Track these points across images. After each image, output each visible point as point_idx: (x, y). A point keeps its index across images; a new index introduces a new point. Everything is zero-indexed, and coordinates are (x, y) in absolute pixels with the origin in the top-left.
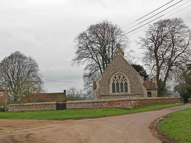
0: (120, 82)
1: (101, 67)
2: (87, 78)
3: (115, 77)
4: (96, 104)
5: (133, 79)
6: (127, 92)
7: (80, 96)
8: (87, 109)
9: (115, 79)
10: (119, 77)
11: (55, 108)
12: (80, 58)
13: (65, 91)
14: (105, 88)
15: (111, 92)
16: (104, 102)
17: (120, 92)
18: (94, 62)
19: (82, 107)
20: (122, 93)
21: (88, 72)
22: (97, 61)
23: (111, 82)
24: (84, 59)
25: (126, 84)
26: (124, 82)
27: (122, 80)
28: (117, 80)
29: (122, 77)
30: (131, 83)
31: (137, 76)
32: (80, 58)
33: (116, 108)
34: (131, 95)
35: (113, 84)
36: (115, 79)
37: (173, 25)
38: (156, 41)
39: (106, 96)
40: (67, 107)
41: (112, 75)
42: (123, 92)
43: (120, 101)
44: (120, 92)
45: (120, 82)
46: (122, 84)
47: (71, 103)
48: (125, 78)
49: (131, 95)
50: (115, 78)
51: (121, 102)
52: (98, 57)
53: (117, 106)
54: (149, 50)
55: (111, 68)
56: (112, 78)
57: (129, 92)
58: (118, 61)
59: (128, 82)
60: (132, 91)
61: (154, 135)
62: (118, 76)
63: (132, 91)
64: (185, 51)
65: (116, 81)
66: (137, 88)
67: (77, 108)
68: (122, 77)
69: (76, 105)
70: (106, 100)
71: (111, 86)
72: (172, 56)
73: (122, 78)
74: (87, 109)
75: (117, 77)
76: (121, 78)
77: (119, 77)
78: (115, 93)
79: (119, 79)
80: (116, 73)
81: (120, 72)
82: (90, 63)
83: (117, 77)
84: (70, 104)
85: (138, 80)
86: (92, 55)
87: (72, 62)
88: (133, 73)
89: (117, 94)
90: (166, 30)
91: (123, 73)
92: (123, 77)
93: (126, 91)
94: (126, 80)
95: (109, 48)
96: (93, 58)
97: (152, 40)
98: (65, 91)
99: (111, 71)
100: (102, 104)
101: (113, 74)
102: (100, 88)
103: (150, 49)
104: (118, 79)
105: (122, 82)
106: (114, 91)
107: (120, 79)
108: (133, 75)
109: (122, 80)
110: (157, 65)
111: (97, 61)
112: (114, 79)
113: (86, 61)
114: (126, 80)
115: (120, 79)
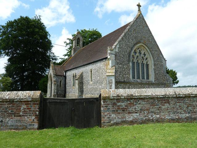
14: (124, 67)
25: (147, 65)
26: (145, 62)
30: (155, 65)
55: (132, 34)
68: (143, 52)
77: (140, 53)
84: (123, 104)
89: (138, 80)
99: (132, 40)
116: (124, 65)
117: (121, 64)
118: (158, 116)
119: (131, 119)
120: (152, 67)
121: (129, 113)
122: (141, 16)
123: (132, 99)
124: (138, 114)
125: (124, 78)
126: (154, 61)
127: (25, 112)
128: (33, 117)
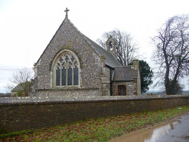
5: (87, 61)
10: (67, 59)
17: (67, 84)
20: (67, 86)
23: (55, 69)
25: (76, 69)
26: (73, 67)
27: (70, 62)
30: (81, 67)
31: (94, 54)
35: (58, 71)
36: (61, 62)
37: (182, 20)
38: (164, 39)
44: (67, 84)
46: (64, 70)
54: (157, 48)
55: (54, 44)
60: (83, 82)
66: (92, 77)
68: (69, 57)
72: (182, 54)
75: (64, 58)
77: (67, 59)
78: (71, 86)
81: (66, 50)
85: (94, 62)
88: (86, 50)
90: (174, 25)
99: (54, 50)
103: (158, 47)
106: (58, 84)
108: (86, 53)
110: (166, 62)
115: (67, 61)
122: (66, 21)
125: (45, 86)
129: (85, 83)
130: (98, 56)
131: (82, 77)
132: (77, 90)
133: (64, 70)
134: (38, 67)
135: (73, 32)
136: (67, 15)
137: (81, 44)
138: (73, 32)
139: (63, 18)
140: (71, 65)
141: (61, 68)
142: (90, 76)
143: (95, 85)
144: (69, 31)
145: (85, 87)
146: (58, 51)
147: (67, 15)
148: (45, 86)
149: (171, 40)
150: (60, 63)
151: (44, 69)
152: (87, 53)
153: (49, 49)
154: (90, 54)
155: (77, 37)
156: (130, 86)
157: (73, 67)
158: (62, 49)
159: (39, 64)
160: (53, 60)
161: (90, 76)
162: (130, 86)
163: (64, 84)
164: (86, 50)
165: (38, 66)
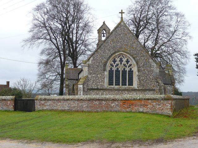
0: (121, 69)
1: (62, 52)
2: (44, 65)
3: (115, 59)
4: (97, 103)
5: (144, 65)
6: (132, 85)
7: (33, 92)
8: (77, 111)
9: (114, 63)
10: (121, 61)
11: (11, 107)
12: (35, 37)
13: (8, 83)
14: (98, 77)
15: (106, 84)
16: (114, 100)
18: (54, 47)
19: (67, 108)
20: (121, 86)
21: (44, 58)
22: (56, 45)
23: (108, 69)
24: (40, 41)
25: (131, 72)
26: (127, 69)
27: (124, 65)
28: (117, 65)
29: (125, 60)
30: (139, 71)
32: (35, 37)
33: (140, 112)
34: (139, 90)
35: (111, 72)
36: (114, 63)
39: (97, 89)
40: (37, 106)
41: (110, 57)
42: (126, 85)
43: (148, 99)
45: (121, 69)
46: (117, 71)
47: (45, 99)
48: (129, 63)
49: (139, 90)
50: (115, 61)
51: (150, 101)
52: (58, 40)
53: (141, 110)
55: (109, 45)
56: (109, 61)
57: (135, 85)
58: (120, 35)
59: (135, 69)
61: (27, 143)
62: (119, 59)
63: (140, 84)
64: (170, 40)
65: (116, 66)
66: (149, 80)
67: (56, 110)
68: (125, 60)
69: (54, 103)
70: (117, 97)
71: (106, 73)
72: (156, 45)
73: (125, 63)
74: (77, 111)
75: (118, 60)
76: (123, 63)
77: (121, 61)
78: (112, 86)
79: (120, 64)
80: (116, 54)
82: (47, 46)
83: (118, 60)
84: (43, 102)
85: (150, 67)
86: (50, 36)
87: (23, 44)
88: (144, 56)
89: (117, 87)
91: (128, 55)
92: (127, 62)
93: (131, 83)
94: (130, 65)
95: (73, 30)
96: (51, 40)
97: (133, 22)
98: (8, 83)
99: (109, 50)
100: (110, 105)
101: (112, 55)
102: (89, 76)
104: (119, 63)
105: (124, 69)
106: (111, 83)
107: (121, 63)
109: (124, 65)
111: (56, 45)
112: (113, 63)
113: (41, 43)
114: (130, 65)
115: (121, 63)
116: (97, 75)
117: (94, 74)
118: (56, 108)
119: (46, 109)
120: (135, 73)
121: (45, 106)
122: (122, 24)
123: (46, 100)
124: (48, 107)
125: (97, 86)
126: (138, 68)
127: (9, 104)
128: (12, 106)
129: (142, 85)
130: (154, 63)
131: (139, 79)
132: (134, 90)
133: (117, 71)
134: (89, 65)
135: (130, 37)
136: (122, 18)
137: (139, 49)
138: (130, 37)
139: (119, 20)
140: (126, 66)
141: (114, 69)
142: (147, 79)
143: (151, 87)
144: (126, 34)
145: (142, 88)
146: (113, 52)
147: (122, 18)
148: (97, 86)
149: (143, 21)
150: (126, 65)
151: (97, 68)
152: (144, 59)
153: (102, 49)
154: (147, 60)
155: (134, 42)
156: (169, 88)
157: (127, 69)
158: (118, 51)
159: (90, 62)
160: (108, 60)
161: (147, 79)
162: (169, 88)
163: (117, 84)
164: (144, 56)
165: (89, 64)
